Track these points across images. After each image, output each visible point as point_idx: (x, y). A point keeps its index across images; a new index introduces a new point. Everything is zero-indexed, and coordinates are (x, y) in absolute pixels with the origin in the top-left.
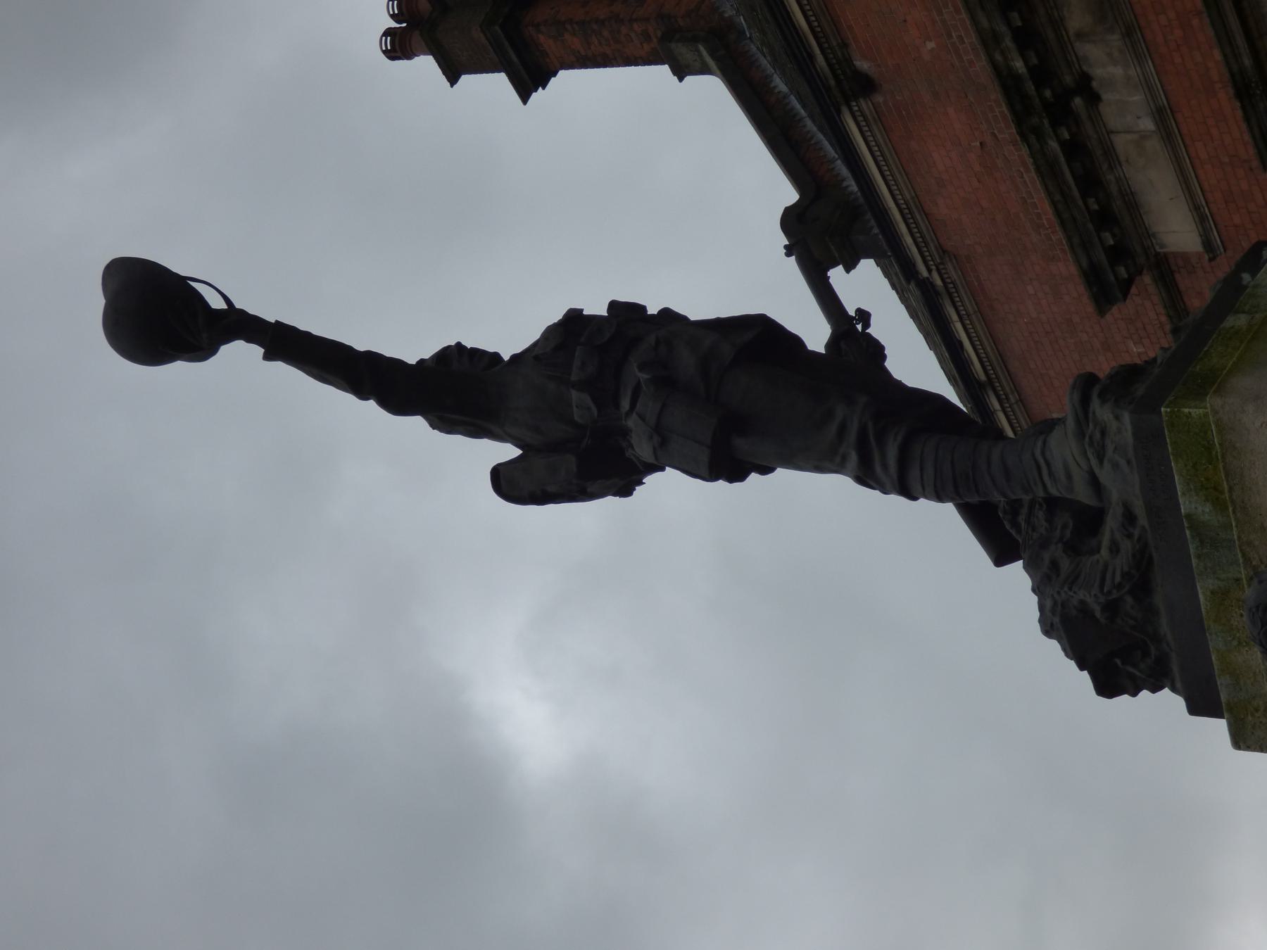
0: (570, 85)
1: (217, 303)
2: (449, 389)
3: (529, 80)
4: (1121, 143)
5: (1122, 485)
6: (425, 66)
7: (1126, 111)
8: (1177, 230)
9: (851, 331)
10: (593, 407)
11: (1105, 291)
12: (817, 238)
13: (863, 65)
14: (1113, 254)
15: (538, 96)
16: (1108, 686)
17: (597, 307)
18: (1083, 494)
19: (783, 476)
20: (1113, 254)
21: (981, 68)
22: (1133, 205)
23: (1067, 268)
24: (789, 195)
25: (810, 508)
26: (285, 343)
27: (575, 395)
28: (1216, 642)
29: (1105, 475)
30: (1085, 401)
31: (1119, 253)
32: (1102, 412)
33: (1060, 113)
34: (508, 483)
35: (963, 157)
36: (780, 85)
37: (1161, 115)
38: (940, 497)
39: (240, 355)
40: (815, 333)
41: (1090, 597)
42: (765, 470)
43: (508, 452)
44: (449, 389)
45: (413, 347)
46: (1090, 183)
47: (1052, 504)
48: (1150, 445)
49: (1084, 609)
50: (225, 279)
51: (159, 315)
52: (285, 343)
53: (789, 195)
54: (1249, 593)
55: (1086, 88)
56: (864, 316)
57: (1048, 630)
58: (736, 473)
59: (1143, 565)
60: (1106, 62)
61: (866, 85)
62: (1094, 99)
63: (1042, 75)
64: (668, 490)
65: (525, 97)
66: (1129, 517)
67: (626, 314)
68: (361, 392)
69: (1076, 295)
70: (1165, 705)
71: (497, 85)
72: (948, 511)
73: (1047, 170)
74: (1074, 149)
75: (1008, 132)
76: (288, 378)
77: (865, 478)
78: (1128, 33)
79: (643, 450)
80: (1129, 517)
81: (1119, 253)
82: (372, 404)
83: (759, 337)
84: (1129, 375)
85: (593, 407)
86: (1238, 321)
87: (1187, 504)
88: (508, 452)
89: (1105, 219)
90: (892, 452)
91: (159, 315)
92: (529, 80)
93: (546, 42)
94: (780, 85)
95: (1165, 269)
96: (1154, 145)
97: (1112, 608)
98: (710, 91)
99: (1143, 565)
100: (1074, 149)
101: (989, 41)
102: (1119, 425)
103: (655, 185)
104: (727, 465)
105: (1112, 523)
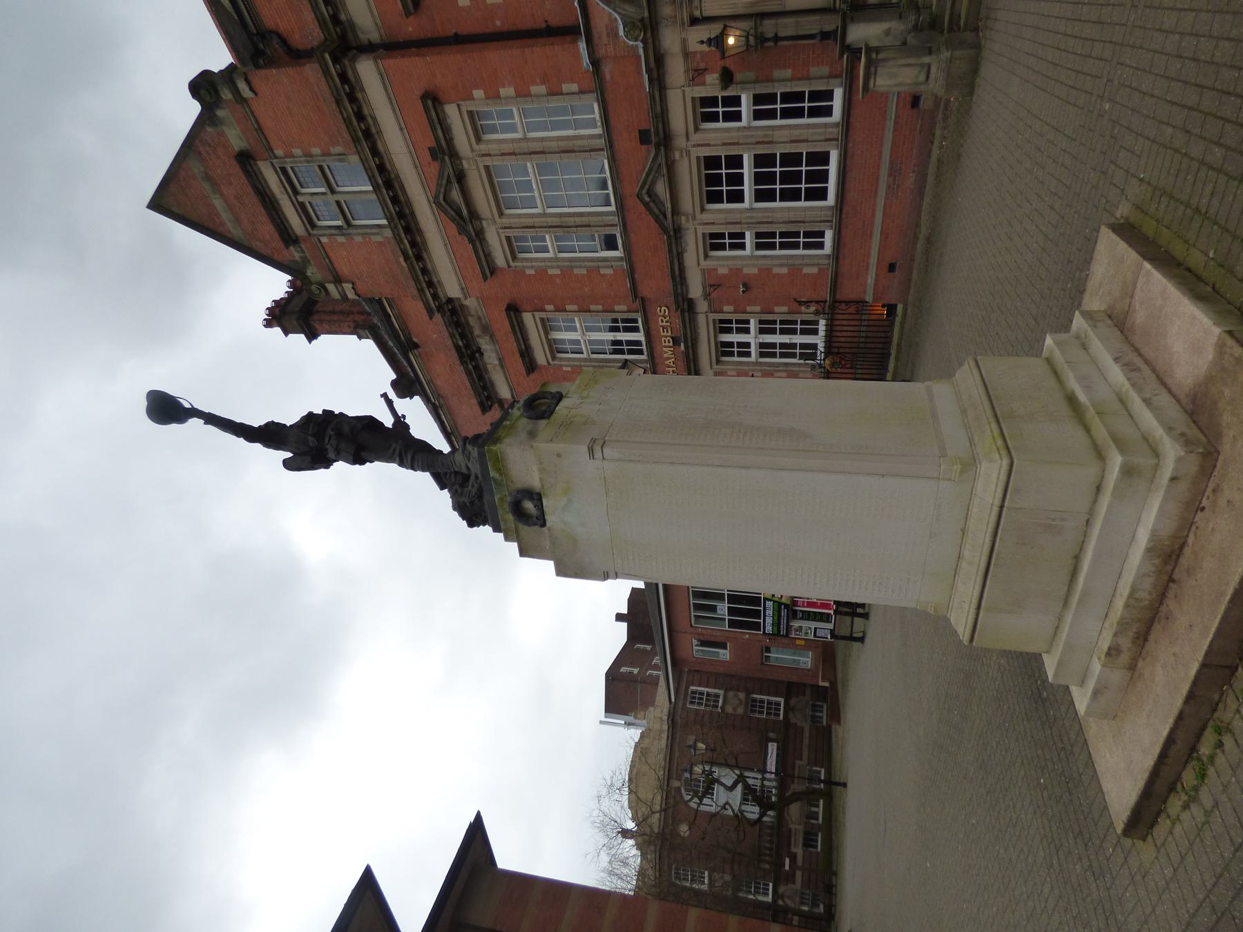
0: (324, 339)
1: (187, 406)
2: (270, 435)
3: (312, 336)
4: (489, 367)
5: (475, 468)
6: (277, 330)
7: (490, 358)
8: (504, 392)
9: (401, 424)
10: (319, 441)
11: (485, 408)
12: (405, 386)
13: (415, 340)
14: (486, 397)
15: (314, 342)
16: (471, 524)
17: (318, 411)
18: (464, 471)
19: (377, 464)
20: (486, 397)
21: (450, 342)
22: (492, 385)
23: (474, 401)
24: (394, 376)
25: (383, 475)
26: (211, 419)
27: (310, 438)
28: (500, 512)
29: (470, 465)
30: (465, 444)
31: (488, 398)
32: (469, 447)
33: (472, 358)
34: (288, 464)
35: (443, 366)
36: (391, 343)
37: (500, 360)
38: (423, 470)
39: (195, 422)
40: (388, 421)
41: (465, 499)
42: (371, 462)
43: (289, 455)
44: (270, 435)
45: (257, 421)
46: (481, 378)
47: (456, 473)
48: (482, 456)
49: (464, 503)
50: (188, 398)
51: (165, 409)
52: (211, 419)
53: (394, 376)
54: (509, 499)
55: (479, 350)
56: (404, 417)
57: (454, 509)
58: (362, 462)
59: (480, 490)
60: (485, 344)
61: (416, 346)
62: (482, 354)
63: (467, 346)
64: (340, 467)
65: (310, 341)
66: (477, 477)
67: (328, 414)
68: (238, 435)
69: (477, 409)
70: (487, 529)
71: (301, 338)
72: (427, 475)
73: (469, 373)
74: (476, 368)
75: (458, 362)
76: (212, 430)
77: (401, 464)
78: (492, 336)
79: (331, 455)
80: (477, 477)
81: (488, 398)
82: (242, 439)
83: (370, 423)
84: (477, 437)
85: (319, 441)
86: (507, 423)
87: (493, 474)
88: (289, 455)
89: (485, 388)
90: (409, 457)
91: (165, 409)
92: (312, 336)
93: (317, 326)
94: (391, 343)
95: (501, 402)
96: (498, 368)
97: (472, 503)
98: (369, 345)
99: (480, 490)
100: (476, 368)
101: (452, 336)
102: (474, 451)
103: (349, 374)
104: (358, 459)
105: (472, 478)
